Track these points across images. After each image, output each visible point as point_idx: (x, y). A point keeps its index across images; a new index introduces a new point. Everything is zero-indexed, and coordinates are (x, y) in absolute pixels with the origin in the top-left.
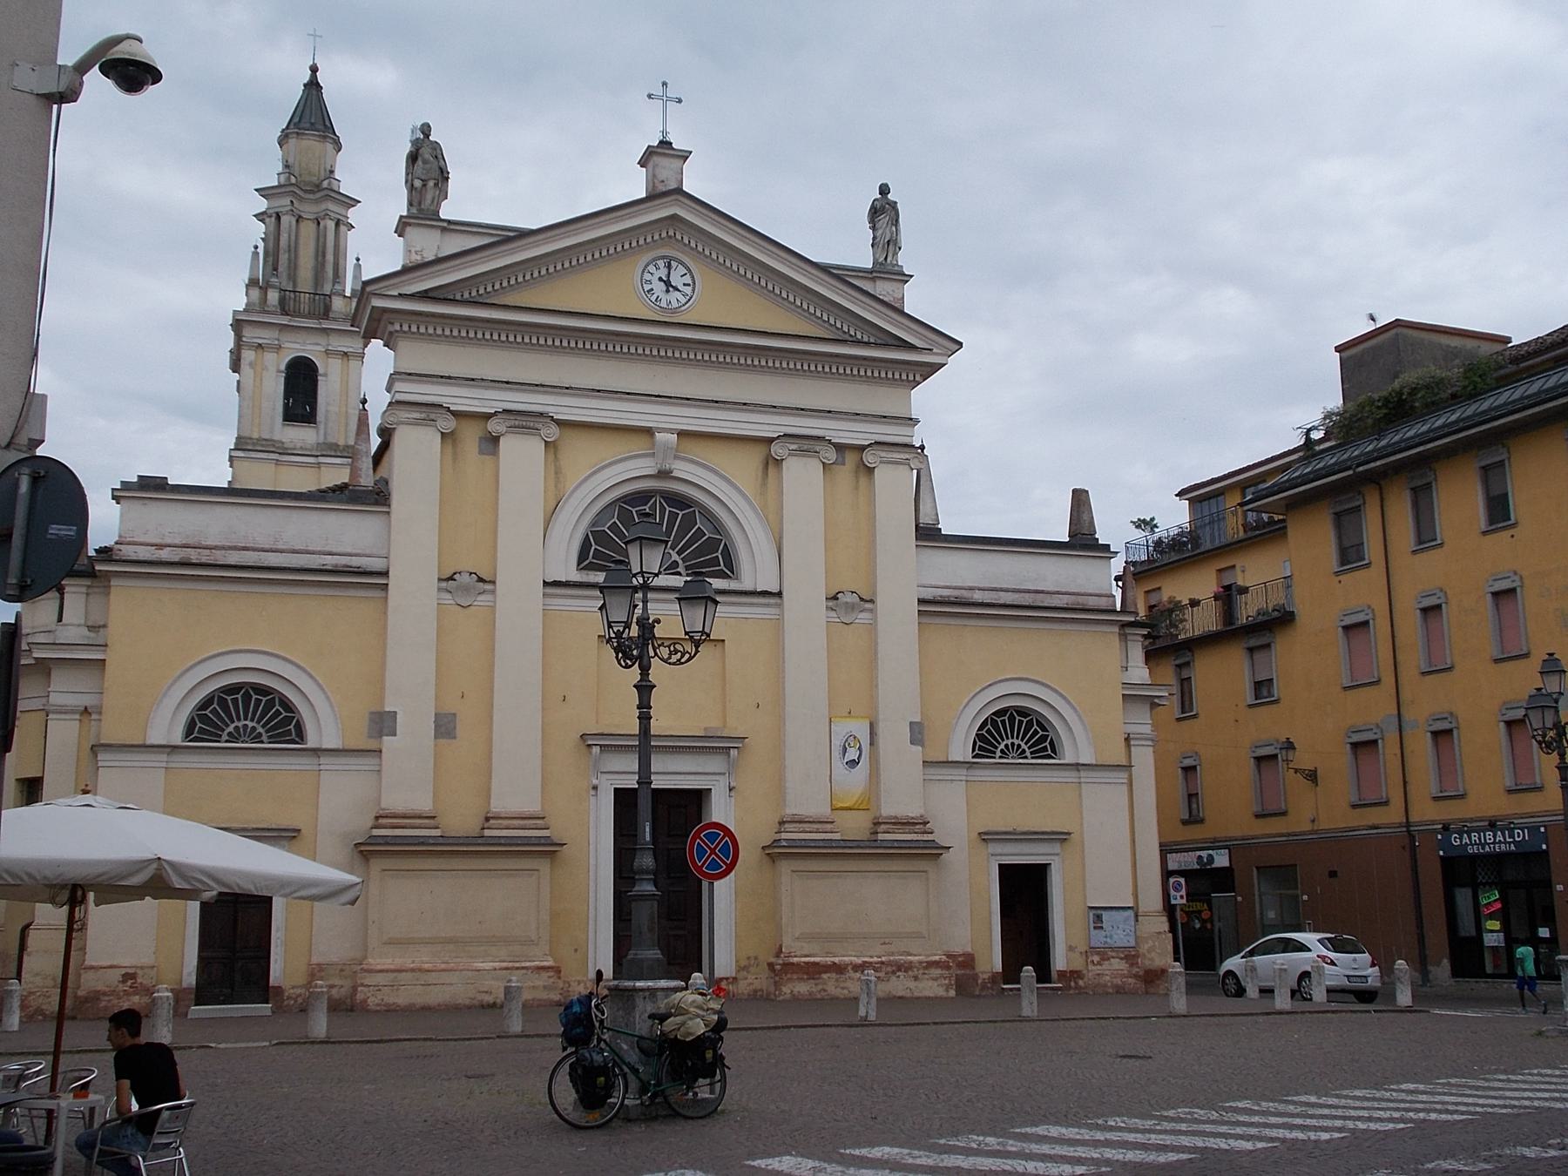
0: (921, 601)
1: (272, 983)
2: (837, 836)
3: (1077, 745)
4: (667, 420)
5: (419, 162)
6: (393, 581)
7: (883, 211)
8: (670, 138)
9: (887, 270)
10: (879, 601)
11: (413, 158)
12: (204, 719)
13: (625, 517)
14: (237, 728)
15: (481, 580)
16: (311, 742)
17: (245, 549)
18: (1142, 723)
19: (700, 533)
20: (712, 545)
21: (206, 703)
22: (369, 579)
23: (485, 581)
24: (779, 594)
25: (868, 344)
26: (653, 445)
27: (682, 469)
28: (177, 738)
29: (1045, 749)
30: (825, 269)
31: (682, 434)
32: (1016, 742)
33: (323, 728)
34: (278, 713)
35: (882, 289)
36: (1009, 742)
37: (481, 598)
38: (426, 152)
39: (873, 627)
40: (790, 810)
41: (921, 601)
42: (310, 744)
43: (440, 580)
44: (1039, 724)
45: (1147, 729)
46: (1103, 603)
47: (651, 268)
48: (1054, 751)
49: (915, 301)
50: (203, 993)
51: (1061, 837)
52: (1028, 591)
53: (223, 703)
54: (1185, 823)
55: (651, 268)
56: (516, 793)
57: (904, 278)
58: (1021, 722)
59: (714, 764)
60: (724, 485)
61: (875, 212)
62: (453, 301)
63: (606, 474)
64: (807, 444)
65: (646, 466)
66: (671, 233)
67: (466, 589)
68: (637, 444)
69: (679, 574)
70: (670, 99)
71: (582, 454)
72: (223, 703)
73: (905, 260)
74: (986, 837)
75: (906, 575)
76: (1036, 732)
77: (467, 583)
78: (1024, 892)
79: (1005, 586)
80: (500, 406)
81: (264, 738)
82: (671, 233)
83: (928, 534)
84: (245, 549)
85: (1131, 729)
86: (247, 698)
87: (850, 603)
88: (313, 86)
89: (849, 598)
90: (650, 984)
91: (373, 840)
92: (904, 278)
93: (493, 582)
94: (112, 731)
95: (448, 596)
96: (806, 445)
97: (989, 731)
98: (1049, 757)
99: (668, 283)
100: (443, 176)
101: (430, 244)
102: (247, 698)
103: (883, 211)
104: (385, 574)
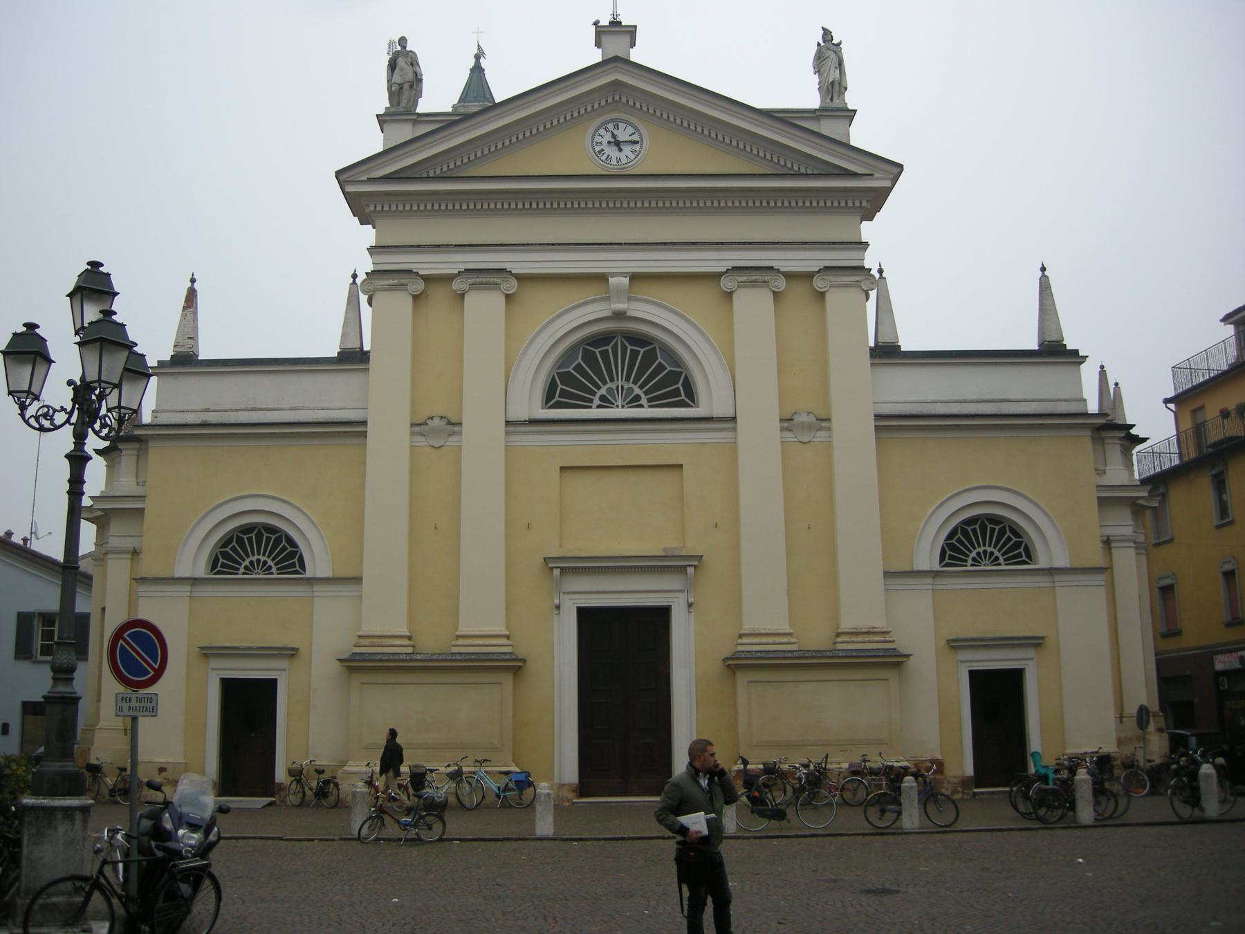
0: (878, 417)
1: (277, 780)
2: (795, 647)
3: (1052, 549)
4: (617, 267)
6: (370, 429)
7: (828, 55)
8: (620, 18)
9: (835, 109)
10: (833, 419)
11: (392, 66)
12: (225, 555)
13: (589, 358)
15: (449, 423)
16: (309, 573)
17: (254, 409)
18: (1123, 525)
20: (674, 377)
21: (226, 541)
22: (352, 430)
23: (454, 425)
25: (806, 175)
27: (638, 309)
28: (201, 570)
31: (635, 277)
33: (318, 563)
35: (828, 128)
36: (981, 550)
37: (450, 439)
41: (878, 417)
43: (412, 425)
47: (602, 131)
48: (1029, 556)
50: (584, 788)
52: (1041, 401)
53: (240, 541)
54: (1229, 625)
55: (602, 131)
56: (482, 618)
57: (850, 115)
60: (674, 320)
62: (428, 179)
63: (564, 320)
66: (617, 98)
68: (591, 292)
71: (541, 302)
72: (240, 541)
73: (851, 99)
74: (956, 645)
75: (859, 396)
77: (437, 428)
78: (997, 700)
79: (1062, 397)
80: (462, 267)
82: (617, 98)
83: (887, 352)
84: (254, 409)
85: (1108, 531)
86: (259, 537)
87: (805, 424)
89: (804, 418)
90: (45, 801)
91: (355, 657)
93: (460, 424)
94: (148, 567)
95: (422, 439)
97: (959, 540)
101: (405, 132)
102: (259, 537)
103: (828, 55)
104: (364, 423)
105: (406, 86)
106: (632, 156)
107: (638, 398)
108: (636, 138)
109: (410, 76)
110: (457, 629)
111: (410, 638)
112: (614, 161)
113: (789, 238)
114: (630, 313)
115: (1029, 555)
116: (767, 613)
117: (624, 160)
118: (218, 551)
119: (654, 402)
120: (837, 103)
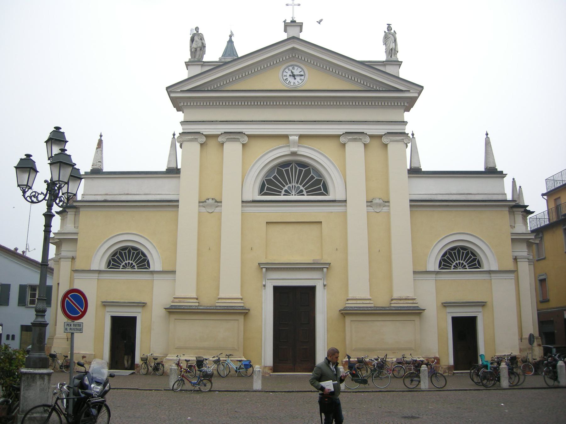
2: (372, 305)
3: (490, 262)
4: (294, 132)
5: (194, 42)
7: (390, 37)
10: (391, 202)
13: (280, 173)
14: (456, 264)
15: (216, 202)
16: (486, 268)
17: (128, 194)
18: (523, 251)
19: (312, 177)
20: (318, 182)
21: (114, 254)
22: (173, 204)
23: (218, 202)
24: (346, 201)
26: (289, 143)
27: (302, 151)
28: (103, 267)
29: (475, 264)
30: (362, 63)
31: (301, 137)
32: (461, 262)
33: (156, 264)
34: (141, 257)
35: (389, 69)
36: (458, 262)
37: (217, 209)
38: (196, 38)
39: (389, 213)
40: (350, 296)
42: (151, 269)
43: (199, 202)
44: (472, 253)
45: (525, 254)
46: (500, 198)
49: (404, 73)
51: (482, 304)
53: (121, 254)
56: (230, 290)
57: (399, 64)
58: (463, 253)
59: (316, 275)
60: (319, 156)
61: (386, 38)
63: (269, 155)
64: (356, 136)
65: (285, 151)
67: (211, 206)
68: (281, 142)
69: (303, 195)
70: (295, 5)
71: (259, 147)
73: (400, 57)
74: (446, 305)
75: (403, 190)
76: (471, 257)
77: (211, 203)
78: (465, 331)
80: (223, 131)
81: (467, 267)
82: (294, 55)
83: (415, 172)
84: (128, 194)
85: (516, 254)
87: (378, 204)
88: (230, 42)
89: (377, 201)
91: (172, 307)
92: (399, 64)
94: (79, 265)
95: (204, 209)
96: (356, 136)
97: (448, 257)
98: (477, 268)
99: (294, 76)
100: (203, 46)
101: (197, 70)
103: (390, 37)
104: (178, 201)
105: (198, 49)
106: (300, 82)
107: (302, 191)
108: (302, 73)
109: (200, 45)
110: (218, 295)
111: (197, 299)
112: (292, 84)
113: (371, 121)
114: (299, 153)
115: (480, 264)
116: (360, 289)
117: (297, 83)
118: (110, 258)
119: (309, 193)
120: (393, 58)
